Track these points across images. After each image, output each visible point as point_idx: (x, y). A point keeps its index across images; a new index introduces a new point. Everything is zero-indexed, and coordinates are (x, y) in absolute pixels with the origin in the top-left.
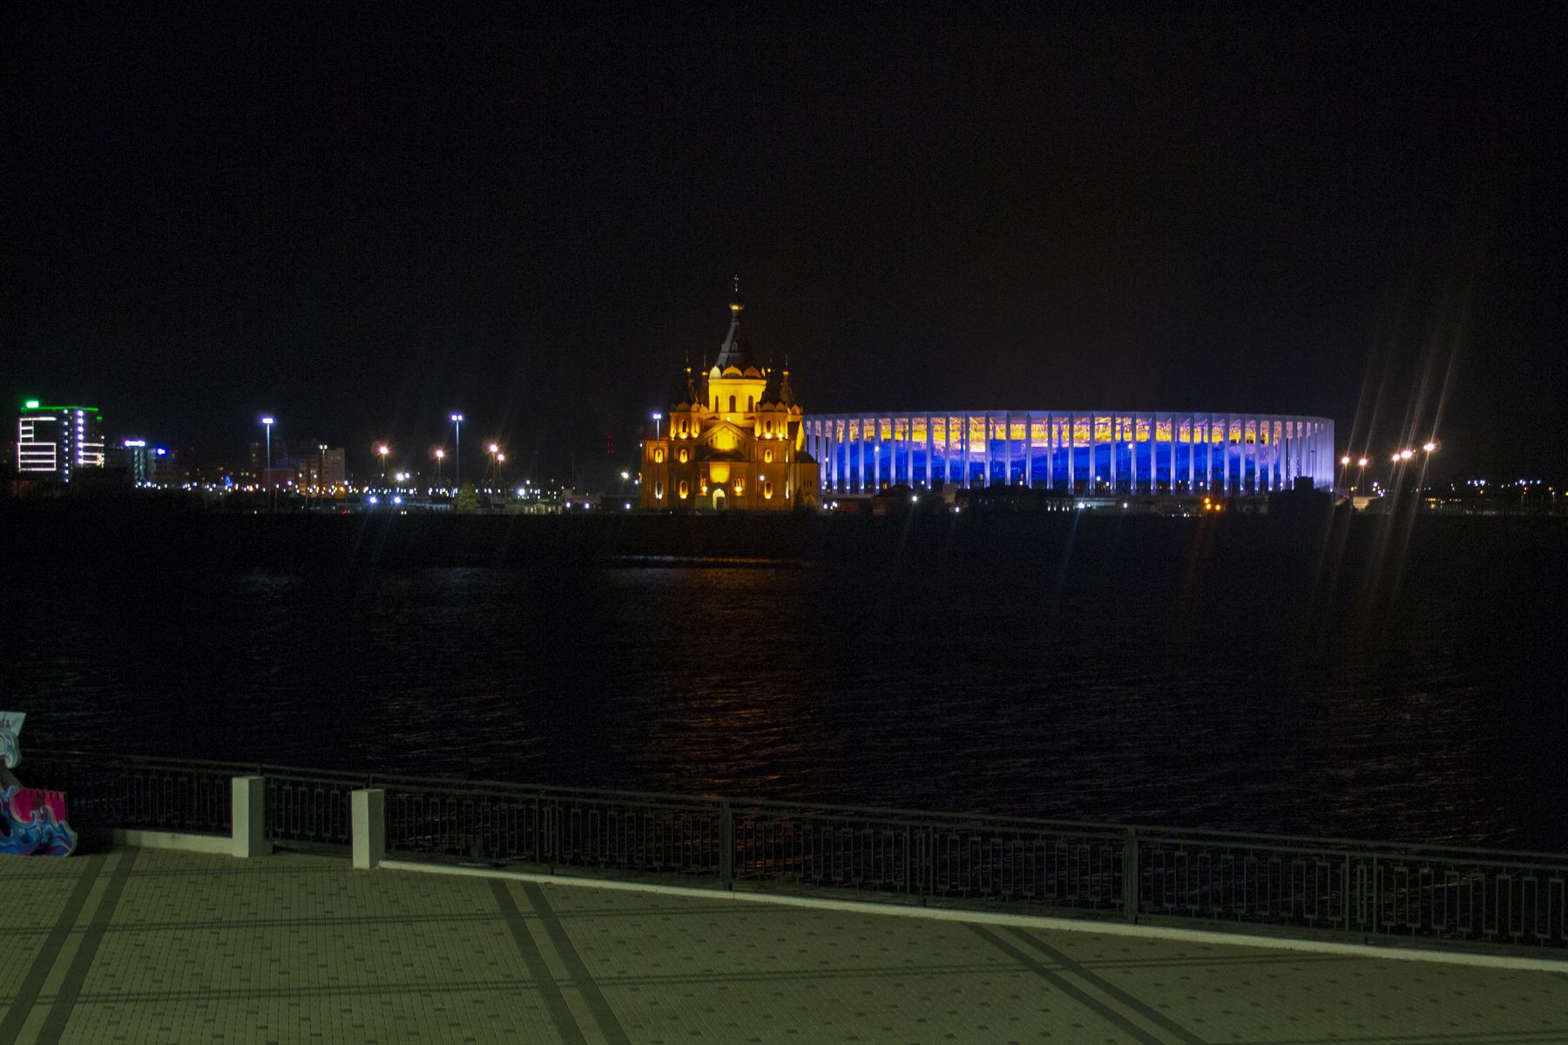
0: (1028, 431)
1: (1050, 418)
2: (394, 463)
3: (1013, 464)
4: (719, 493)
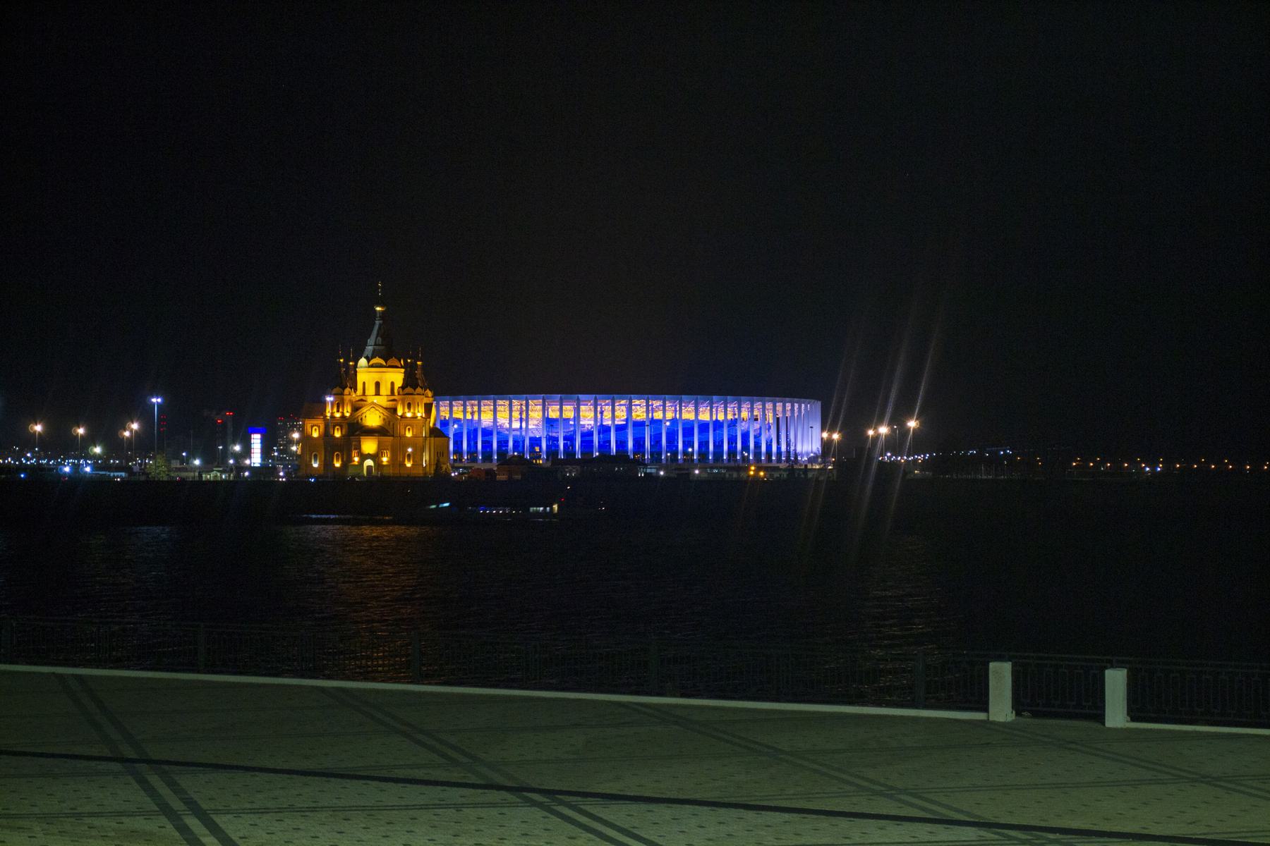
0: (577, 411)
1: (596, 400)
2: (90, 439)
3: (565, 438)
4: (369, 462)
